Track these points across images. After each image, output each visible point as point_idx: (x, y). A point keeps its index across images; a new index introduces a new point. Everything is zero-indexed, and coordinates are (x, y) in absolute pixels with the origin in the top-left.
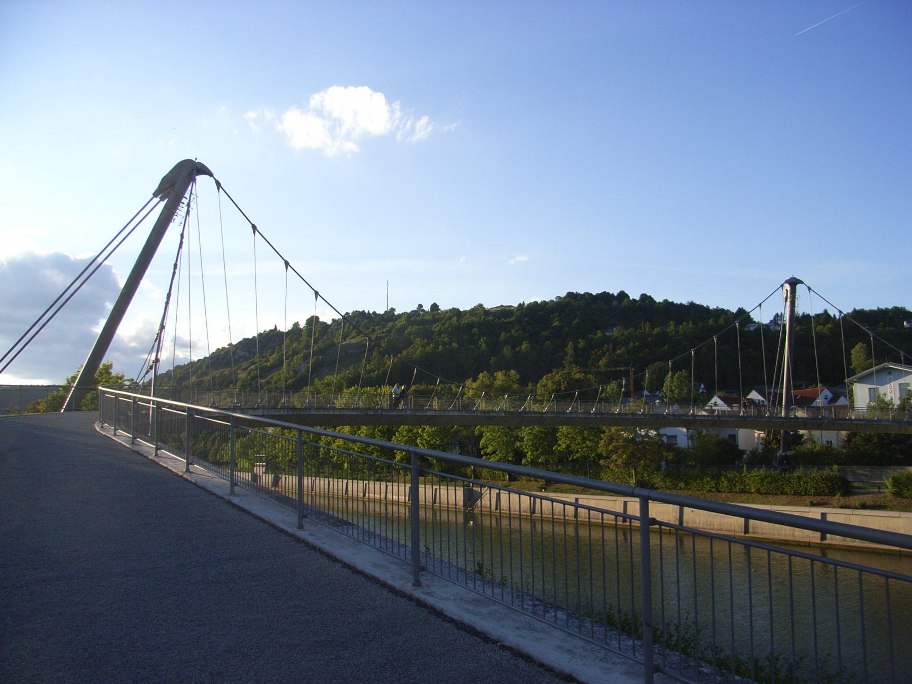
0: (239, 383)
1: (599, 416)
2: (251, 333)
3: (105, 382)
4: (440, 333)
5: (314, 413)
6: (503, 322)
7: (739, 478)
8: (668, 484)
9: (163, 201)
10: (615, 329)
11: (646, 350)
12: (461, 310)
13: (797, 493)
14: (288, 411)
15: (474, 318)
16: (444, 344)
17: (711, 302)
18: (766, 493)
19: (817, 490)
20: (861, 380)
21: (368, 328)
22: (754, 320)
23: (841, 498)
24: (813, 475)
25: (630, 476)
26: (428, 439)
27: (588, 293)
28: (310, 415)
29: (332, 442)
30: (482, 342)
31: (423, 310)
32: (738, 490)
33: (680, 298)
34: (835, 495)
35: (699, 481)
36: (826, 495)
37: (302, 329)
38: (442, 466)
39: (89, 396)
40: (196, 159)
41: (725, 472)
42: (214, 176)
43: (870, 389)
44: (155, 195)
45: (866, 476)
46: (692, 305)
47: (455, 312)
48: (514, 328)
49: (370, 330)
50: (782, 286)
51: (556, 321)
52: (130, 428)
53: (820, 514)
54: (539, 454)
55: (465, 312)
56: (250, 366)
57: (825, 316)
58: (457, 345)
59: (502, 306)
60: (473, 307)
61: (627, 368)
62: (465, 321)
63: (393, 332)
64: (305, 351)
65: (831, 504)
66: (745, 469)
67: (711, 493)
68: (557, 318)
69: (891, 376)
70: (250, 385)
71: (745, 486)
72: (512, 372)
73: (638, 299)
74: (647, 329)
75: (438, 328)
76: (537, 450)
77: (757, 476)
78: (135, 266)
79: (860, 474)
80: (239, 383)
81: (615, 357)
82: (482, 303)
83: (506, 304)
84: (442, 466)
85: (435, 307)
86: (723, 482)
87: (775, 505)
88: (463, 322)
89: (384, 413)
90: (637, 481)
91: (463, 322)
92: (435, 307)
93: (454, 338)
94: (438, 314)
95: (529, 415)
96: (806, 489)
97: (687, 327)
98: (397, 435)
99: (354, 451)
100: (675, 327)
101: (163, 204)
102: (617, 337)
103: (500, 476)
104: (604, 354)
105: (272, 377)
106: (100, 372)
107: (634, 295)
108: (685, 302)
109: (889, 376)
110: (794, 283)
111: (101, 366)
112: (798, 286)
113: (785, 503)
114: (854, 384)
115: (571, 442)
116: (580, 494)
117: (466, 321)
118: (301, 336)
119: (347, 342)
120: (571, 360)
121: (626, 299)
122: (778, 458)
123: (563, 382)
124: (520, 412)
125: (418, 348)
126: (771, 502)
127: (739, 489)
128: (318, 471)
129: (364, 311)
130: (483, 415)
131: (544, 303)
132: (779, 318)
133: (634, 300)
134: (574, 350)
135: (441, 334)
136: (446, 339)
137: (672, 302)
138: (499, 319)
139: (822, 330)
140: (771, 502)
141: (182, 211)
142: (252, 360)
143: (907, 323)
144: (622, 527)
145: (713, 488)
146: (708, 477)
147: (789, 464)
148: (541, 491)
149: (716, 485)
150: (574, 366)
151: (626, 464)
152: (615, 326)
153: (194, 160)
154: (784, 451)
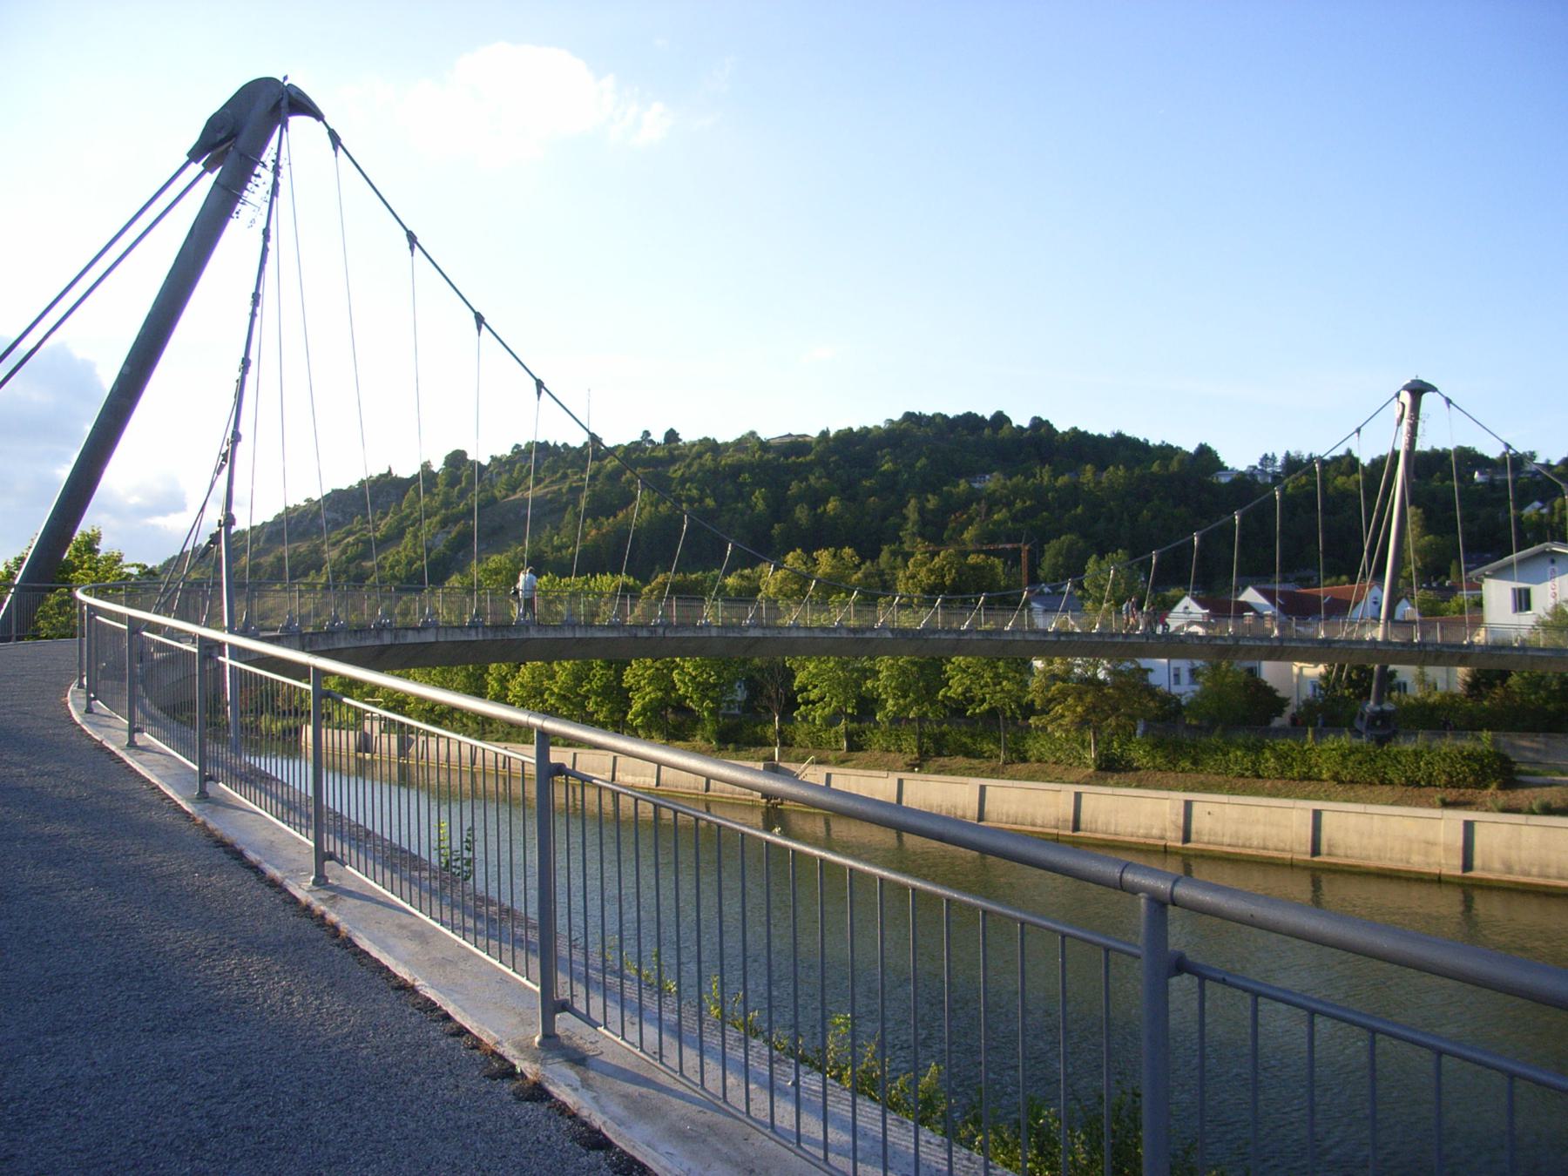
0: (327, 568)
1: (1063, 638)
2: (347, 477)
3: (90, 568)
4: (683, 481)
5: (536, 636)
6: (794, 462)
7: (1299, 752)
8: (1158, 760)
9: (212, 172)
10: (987, 477)
11: (1045, 514)
12: (720, 441)
13: (1413, 783)
14: (484, 633)
15: (743, 456)
16: (690, 500)
17: (1154, 436)
18: (1352, 782)
19: (1452, 777)
20: (1497, 574)
21: (555, 472)
22: (1226, 465)
23: (1499, 792)
24: (1445, 749)
25: (1084, 745)
26: (694, 674)
27: (940, 414)
28: (529, 639)
29: (509, 677)
30: (758, 499)
31: (652, 442)
32: (1296, 775)
33: (1100, 425)
34: (1486, 787)
35: (1220, 756)
36: (1467, 787)
37: (437, 473)
38: (718, 722)
39: (53, 599)
40: (285, 78)
41: (1271, 741)
42: (326, 119)
43: (1514, 590)
44: (194, 155)
45: (1537, 751)
46: (1120, 438)
47: (709, 446)
48: (814, 474)
49: (559, 475)
50: (1398, 395)
51: (887, 462)
52: (192, 747)
53: (1461, 823)
54: (910, 703)
55: (726, 444)
56: (344, 539)
57: (1348, 459)
58: (713, 503)
59: (790, 435)
60: (739, 436)
61: (1015, 546)
62: (726, 460)
63: (601, 478)
64: (443, 511)
65: (1481, 804)
66: (1310, 736)
67: (1242, 779)
68: (887, 458)
69: (1556, 568)
70: (345, 572)
71: (1310, 768)
72: (847, 551)
73: (1026, 424)
74: (1046, 478)
75: (680, 473)
76: (905, 696)
77: (1333, 750)
78: (149, 315)
79: (1524, 748)
80: (327, 568)
81: (990, 526)
82: (755, 429)
83: (797, 431)
84: (718, 722)
85: (672, 436)
86: (1267, 760)
87: (1372, 803)
88: (723, 462)
89: (668, 634)
90: (1100, 755)
91: (723, 462)
92: (672, 436)
93: (708, 491)
94: (678, 448)
95: (937, 636)
96: (1431, 775)
97: (1116, 474)
98: (635, 666)
99: (552, 694)
100: (1094, 474)
101: (210, 179)
102: (995, 491)
103: (830, 742)
104: (970, 521)
105: (385, 558)
106: (77, 549)
107: (1021, 419)
108: (1108, 433)
109: (1552, 567)
110: (1418, 390)
111: (77, 535)
112: (1427, 398)
113: (1390, 802)
114: (1486, 580)
115: (972, 683)
116: (987, 777)
117: (729, 461)
118: (436, 485)
119: (518, 495)
120: (914, 530)
121: (1006, 427)
122: (1366, 717)
123: (949, 570)
124: (920, 631)
125: (641, 509)
126: (1362, 798)
127: (1298, 772)
128: (484, 730)
129: (546, 442)
130: (852, 636)
131: (865, 432)
132: (1269, 462)
133: (1020, 427)
134: (919, 512)
135: (685, 484)
136: (695, 491)
137: (1085, 433)
138: (787, 458)
139: (1344, 483)
140: (1362, 798)
141: (256, 192)
142: (349, 527)
143: (1481, 474)
144: (1071, 839)
145: (1247, 769)
146: (1238, 748)
147: (1386, 727)
148: (913, 771)
149: (1254, 763)
150: (919, 540)
151: (1083, 723)
152: (990, 472)
153: (282, 80)
154: (1379, 702)
